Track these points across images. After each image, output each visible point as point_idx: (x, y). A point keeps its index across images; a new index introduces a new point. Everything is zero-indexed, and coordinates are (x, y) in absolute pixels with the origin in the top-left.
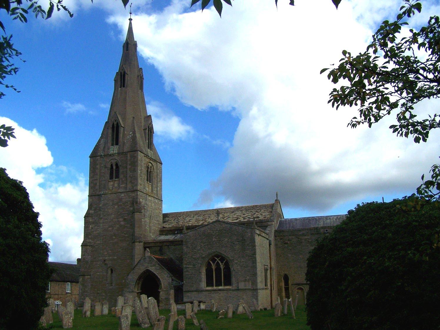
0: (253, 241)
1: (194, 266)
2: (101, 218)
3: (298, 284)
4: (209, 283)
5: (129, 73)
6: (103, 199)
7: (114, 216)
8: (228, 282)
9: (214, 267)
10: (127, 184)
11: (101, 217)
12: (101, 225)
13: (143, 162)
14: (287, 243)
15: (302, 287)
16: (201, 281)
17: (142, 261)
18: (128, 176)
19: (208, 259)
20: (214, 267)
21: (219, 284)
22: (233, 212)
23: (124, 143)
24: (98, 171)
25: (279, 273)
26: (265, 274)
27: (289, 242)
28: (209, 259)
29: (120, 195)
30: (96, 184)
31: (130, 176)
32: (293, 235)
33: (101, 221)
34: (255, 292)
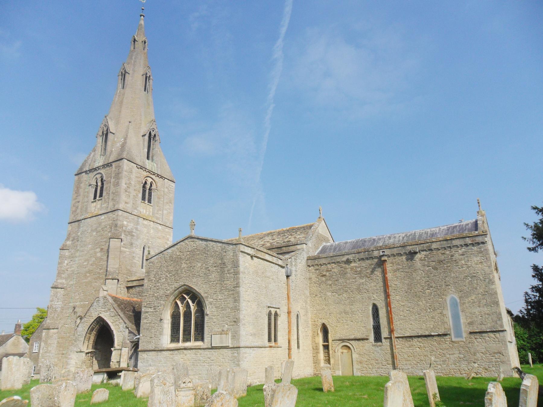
0: (236, 265)
1: (155, 309)
2: (78, 250)
3: (343, 340)
4: (175, 338)
5: (131, 72)
6: (82, 225)
7: (91, 246)
8: (200, 335)
9: (182, 309)
10: (108, 203)
11: (78, 248)
12: (77, 259)
13: (133, 176)
14: (325, 275)
15: (348, 344)
16: (161, 333)
17: (95, 304)
18: (111, 191)
19: (174, 298)
20: (182, 309)
21: (187, 339)
22: (261, 238)
23: (112, 151)
24: (81, 191)
25: (315, 322)
26: (269, 324)
27: (328, 274)
28: (175, 298)
29: (100, 218)
30: (77, 207)
31: (113, 193)
32: (332, 263)
33: (77, 254)
34: (236, 352)
